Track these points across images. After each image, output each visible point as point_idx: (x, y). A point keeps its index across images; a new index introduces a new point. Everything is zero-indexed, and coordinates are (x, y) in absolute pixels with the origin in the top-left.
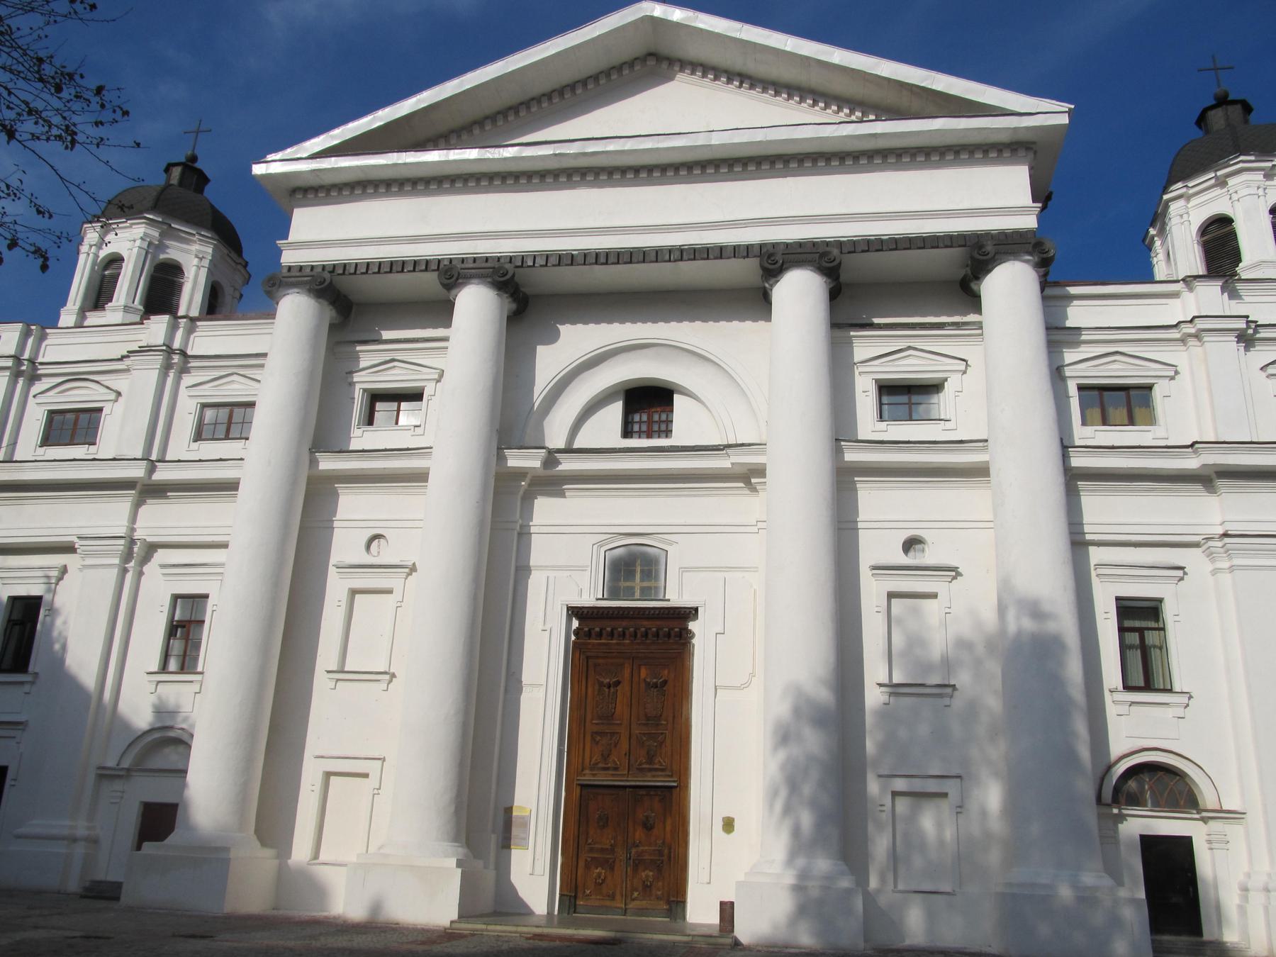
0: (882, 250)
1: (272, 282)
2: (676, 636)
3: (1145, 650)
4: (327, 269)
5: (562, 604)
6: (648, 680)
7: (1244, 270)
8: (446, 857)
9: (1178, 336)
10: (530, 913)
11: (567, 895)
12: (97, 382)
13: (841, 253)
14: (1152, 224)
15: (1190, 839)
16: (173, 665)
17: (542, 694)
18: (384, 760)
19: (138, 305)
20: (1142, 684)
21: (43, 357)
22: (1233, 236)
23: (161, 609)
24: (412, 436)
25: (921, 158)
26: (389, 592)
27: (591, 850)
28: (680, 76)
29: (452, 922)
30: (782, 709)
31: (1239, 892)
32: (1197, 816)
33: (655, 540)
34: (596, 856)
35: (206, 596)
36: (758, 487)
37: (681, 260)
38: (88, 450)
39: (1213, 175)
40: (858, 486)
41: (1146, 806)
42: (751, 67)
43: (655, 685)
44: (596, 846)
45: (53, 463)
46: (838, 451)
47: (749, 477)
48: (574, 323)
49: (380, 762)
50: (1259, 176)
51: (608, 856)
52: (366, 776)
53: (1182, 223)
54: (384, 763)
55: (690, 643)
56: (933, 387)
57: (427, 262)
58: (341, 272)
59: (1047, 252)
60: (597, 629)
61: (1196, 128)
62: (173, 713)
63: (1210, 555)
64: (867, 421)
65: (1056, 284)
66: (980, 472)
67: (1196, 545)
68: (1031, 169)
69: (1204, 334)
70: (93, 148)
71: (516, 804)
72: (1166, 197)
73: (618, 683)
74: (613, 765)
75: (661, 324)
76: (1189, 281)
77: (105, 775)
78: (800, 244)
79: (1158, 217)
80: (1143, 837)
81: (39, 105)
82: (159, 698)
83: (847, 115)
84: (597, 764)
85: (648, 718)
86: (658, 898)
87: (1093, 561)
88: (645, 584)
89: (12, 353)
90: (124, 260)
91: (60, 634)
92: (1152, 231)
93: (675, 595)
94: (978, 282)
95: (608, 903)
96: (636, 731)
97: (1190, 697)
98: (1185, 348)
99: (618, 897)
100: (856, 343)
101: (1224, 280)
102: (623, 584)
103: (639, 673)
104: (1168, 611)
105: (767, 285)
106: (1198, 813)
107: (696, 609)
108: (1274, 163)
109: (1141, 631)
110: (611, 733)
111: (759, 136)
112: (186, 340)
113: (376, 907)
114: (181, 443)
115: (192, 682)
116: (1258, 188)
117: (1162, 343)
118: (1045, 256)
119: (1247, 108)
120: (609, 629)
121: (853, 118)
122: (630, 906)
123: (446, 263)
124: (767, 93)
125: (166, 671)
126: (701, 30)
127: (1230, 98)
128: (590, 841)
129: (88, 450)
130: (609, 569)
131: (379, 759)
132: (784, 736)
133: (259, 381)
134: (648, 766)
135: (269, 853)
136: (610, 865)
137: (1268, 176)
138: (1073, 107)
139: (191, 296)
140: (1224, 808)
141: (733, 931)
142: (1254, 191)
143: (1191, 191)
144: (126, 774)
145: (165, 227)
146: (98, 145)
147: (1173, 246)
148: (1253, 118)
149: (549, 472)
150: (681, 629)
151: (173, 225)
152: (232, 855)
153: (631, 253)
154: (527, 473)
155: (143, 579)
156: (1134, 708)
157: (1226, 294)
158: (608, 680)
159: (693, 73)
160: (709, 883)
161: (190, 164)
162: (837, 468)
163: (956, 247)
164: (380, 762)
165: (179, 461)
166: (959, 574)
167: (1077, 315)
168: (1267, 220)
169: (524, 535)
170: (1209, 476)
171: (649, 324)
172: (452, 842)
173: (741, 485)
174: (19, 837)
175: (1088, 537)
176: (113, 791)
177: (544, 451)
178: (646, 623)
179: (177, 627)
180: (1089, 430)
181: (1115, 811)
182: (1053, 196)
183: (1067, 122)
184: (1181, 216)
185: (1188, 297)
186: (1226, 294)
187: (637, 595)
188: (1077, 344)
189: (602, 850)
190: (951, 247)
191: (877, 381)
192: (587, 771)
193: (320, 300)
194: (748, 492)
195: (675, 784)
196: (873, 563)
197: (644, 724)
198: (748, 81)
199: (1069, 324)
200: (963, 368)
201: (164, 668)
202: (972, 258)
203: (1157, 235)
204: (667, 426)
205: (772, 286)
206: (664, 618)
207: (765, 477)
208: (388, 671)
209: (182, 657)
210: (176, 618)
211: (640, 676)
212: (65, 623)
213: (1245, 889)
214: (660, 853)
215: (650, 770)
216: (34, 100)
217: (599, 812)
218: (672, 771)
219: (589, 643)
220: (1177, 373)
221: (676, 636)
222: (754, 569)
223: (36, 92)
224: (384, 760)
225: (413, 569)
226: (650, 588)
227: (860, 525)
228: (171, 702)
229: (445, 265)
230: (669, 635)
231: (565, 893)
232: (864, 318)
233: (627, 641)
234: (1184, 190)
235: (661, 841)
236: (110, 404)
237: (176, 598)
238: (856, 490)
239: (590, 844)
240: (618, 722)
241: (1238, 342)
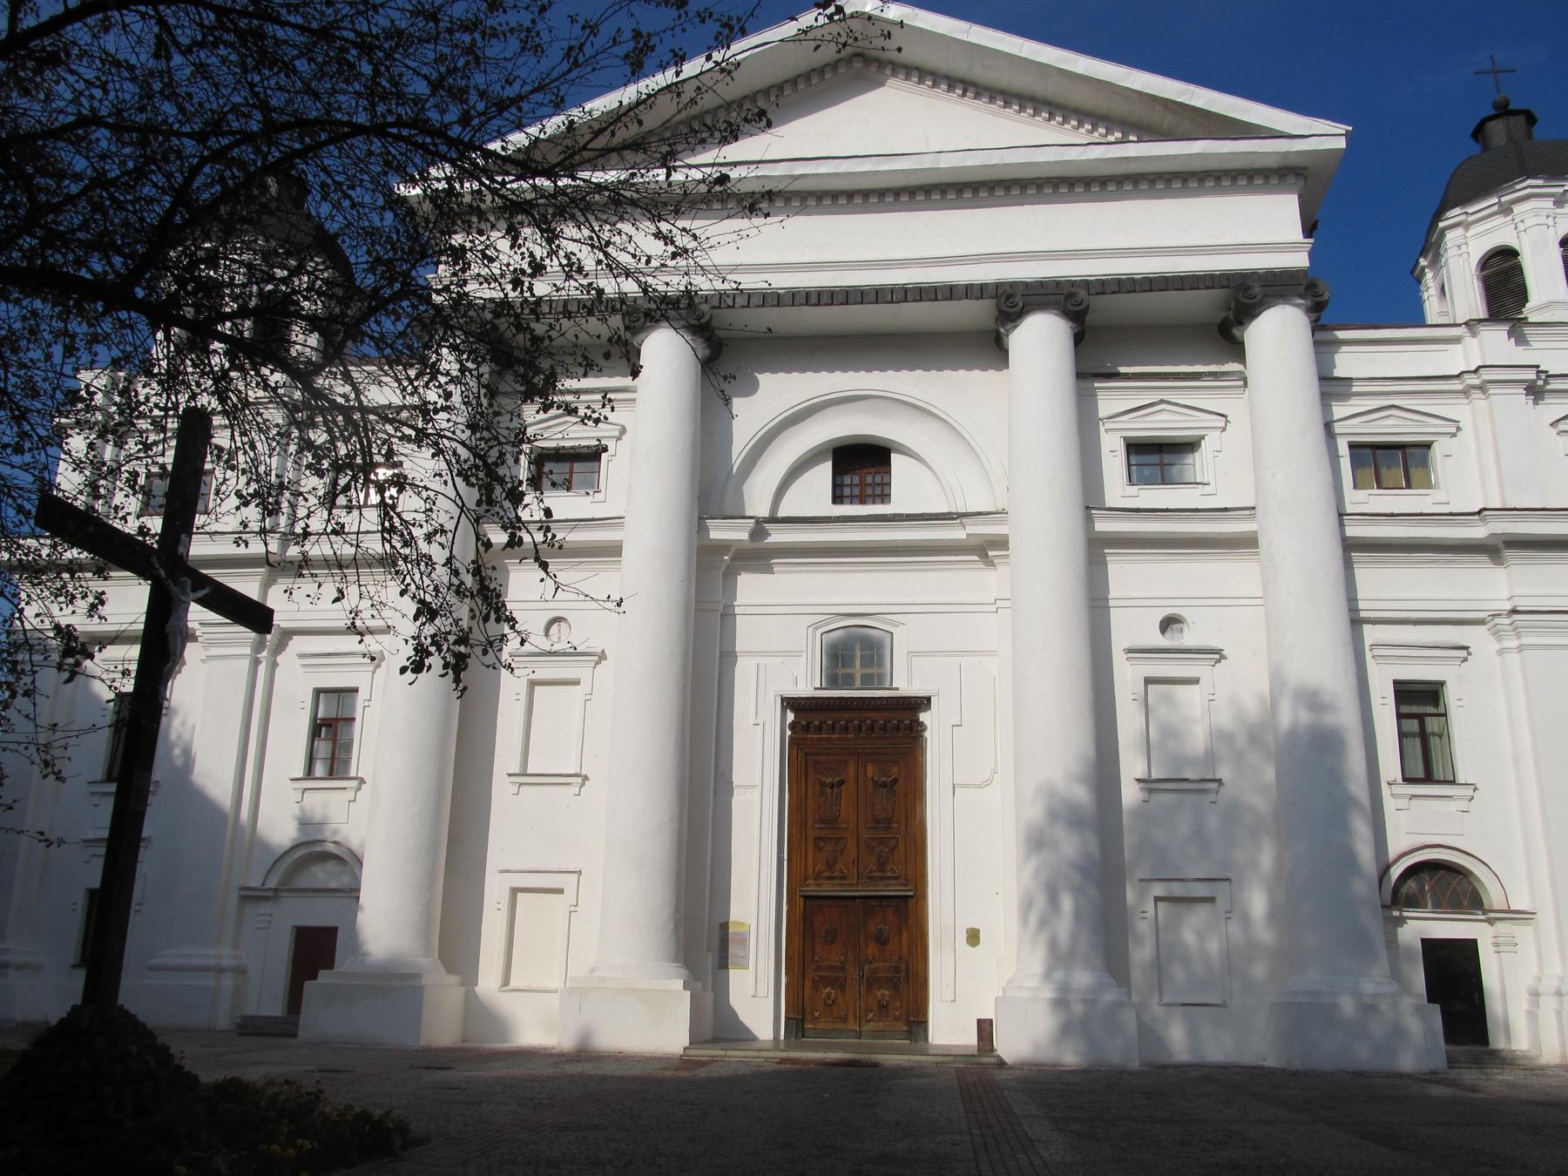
0: (1135, 291)
2: (906, 729)
3: (1424, 736)
5: (775, 695)
7: (1532, 313)
8: (669, 978)
9: (1460, 387)
10: (754, 1038)
13: (1089, 294)
14: (1423, 253)
15: (1474, 942)
16: (320, 769)
17: (757, 797)
18: (580, 873)
20: (1421, 775)
22: (1518, 270)
23: (303, 705)
25: (1177, 185)
26: (576, 682)
27: (819, 968)
28: (891, 82)
29: (685, 1049)
30: (1035, 812)
31: (1528, 997)
32: (1483, 917)
34: (824, 974)
35: (356, 690)
36: (995, 561)
37: (906, 301)
39: (1496, 200)
40: (1108, 558)
41: (1426, 907)
42: (978, 73)
43: (884, 785)
44: (824, 963)
46: (1089, 520)
47: (986, 550)
48: (774, 371)
49: (576, 875)
50: (1548, 203)
51: (837, 975)
52: (560, 891)
53: (1460, 255)
55: (922, 736)
56: (1188, 446)
60: (817, 723)
61: (1471, 141)
62: (321, 825)
63: (1497, 633)
64: (1117, 487)
65: (1324, 328)
66: (1246, 543)
67: (1481, 622)
69: (1489, 386)
71: (732, 919)
72: (1441, 225)
73: (842, 783)
75: (876, 373)
76: (1472, 325)
77: (249, 897)
78: (1042, 284)
79: (1430, 245)
80: (1425, 942)
82: (302, 809)
83: (1088, 131)
85: (878, 822)
86: (896, 1019)
87: (1368, 642)
91: (179, 736)
92: (1423, 262)
93: (904, 683)
95: (840, 1026)
96: (865, 836)
97: (1475, 789)
98: (1466, 401)
99: (851, 1018)
100: (1101, 395)
101: (1511, 324)
102: (840, 671)
103: (866, 771)
104: (1451, 696)
105: (1002, 330)
106: (1483, 914)
107: (929, 699)
108: (1566, 188)
109: (1420, 717)
111: (995, 159)
113: (586, 1037)
115: (345, 789)
116: (1548, 217)
117: (1447, 396)
118: (1318, 299)
119: (1531, 119)
120: (830, 722)
121: (1111, 138)
124: (995, 103)
127: (1512, 107)
128: (817, 958)
130: (827, 654)
131: (574, 872)
132: (1036, 842)
134: (879, 874)
135: (453, 979)
136: (839, 983)
137: (1559, 202)
138: (1350, 128)
140: (1512, 908)
142: (1543, 220)
143: (1471, 218)
144: (275, 895)
148: (1536, 129)
149: (756, 545)
150: (912, 721)
152: (424, 982)
153: (847, 292)
155: (278, 670)
156: (1414, 802)
157: (1513, 339)
158: (830, 780)
159: (921, 82)
160: (954, 1001)
166: (1223, 657)
167: (1347, 363)
168: (1556, 253)
169: (728, 616)
170: (1496, 546)
171: (851, 373)
173: (976, 558)
174: (152, 969)
175: (1363, 614)
176: (259, 915)
177: (753, 521)
178: (871, 714)
179: (321, 726)
180: (1362, 494)
181: (1396, 913)
182: (1319, 226)
183: (1344, 146)
184: (1459, 247)
185: (1471, 343)
186: (1513, 339)
187: (858, 683)
188: (1346, 396)
189: (831, 968)
190: (1213, 288)
191: (1125, 438)
192: (810, 882)
194: (983, 566)
195: (911, 894)
196: (1126, 646)
197: (874, 828)
198: (974, 90)
199: (1337, 373)
201: (309, 773)
203: (1429, 266)
206: (893, 709)
207: (1008, 550)
210: (319, 716)
211: (866, 775)
212: (184, 724)
213: (1535, 994)
214: (897, 970)
215: (882, 878)
219: (808, 739)
220: (1459, 429)
221: (906, 729)
222: (993, 653)
224: (580, 873)
225: (602, 656)
226: (872, 675)
227: (1111, 603)
228: (318, 815)
230: (846, 729)
231: (791, 1016)
232: (1108, 367)
234: (1463, 217)
237: (318, 692)
238: (1105, 563)
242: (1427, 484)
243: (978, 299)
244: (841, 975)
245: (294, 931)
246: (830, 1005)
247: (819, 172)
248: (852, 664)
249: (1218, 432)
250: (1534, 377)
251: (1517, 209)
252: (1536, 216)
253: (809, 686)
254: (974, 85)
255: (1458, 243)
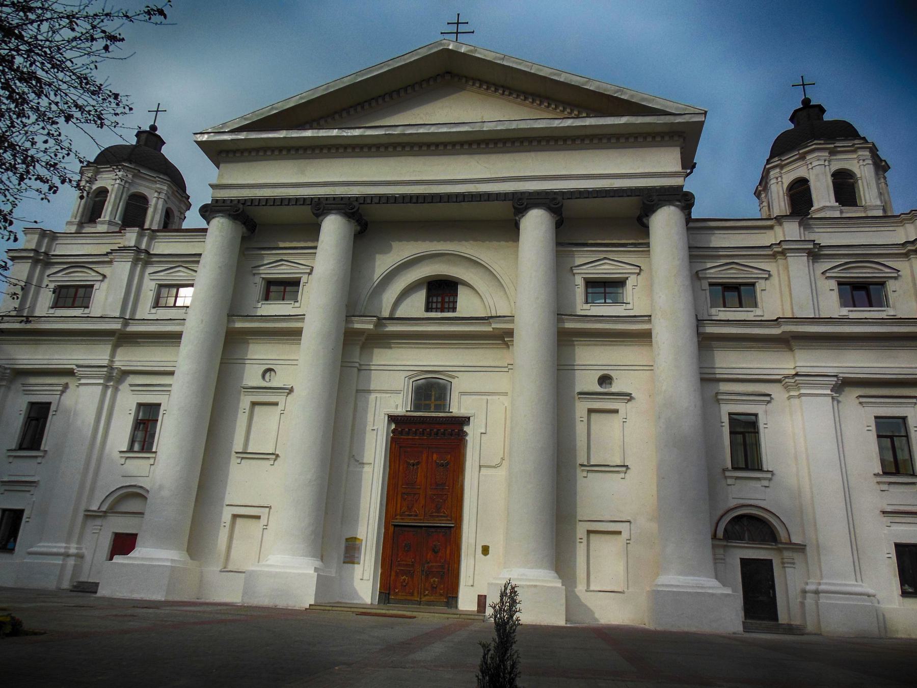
1: (205, 209)
4: (241, 202)
6: (438, 461)
9: (771, 253)
11: (383, 593)
12: (91, 269)
17: (371, 470)
19: (118, 220)
21: (153, 250)
22: (808, 190)
24: (293, 307)
33: (444, 375)
35: (159, 405)
36: (509, 343)
37: (464, 201)
38: (84, 311)
39: (797, 153)
44: (403, 563)
45: (73, 318)
54: (271, 510)
57: (304, 199)
58: (250, 204)
59: (689, 200)
67: (778, 381)
68: (682, 148)
70: (112, 128)
73: (418, 463)
74: (415, 514)
76: (779, 219)
77: (90, 516)
81: (80, 102)
84: (404, 512)
86: (441, 595)
88: (438, 402)
89: (33, 247)
90: (108, 191)
93: (457, 407)
94: (647, 218)
95: (409, 598)
97: (773, 475)
99: (416, 594)
105: (517, 218)
107: (469, 418)
110: (414, 494)
112: (149, 244)
114: (145, 310)
116: (825, 161)
117: (747, 257)
118: (688, 202)
120: (414, 430)
121: (573, 115)
122: (423, 600)
123: (317, 200)
125: (132, 450)
126: (479, 58)
129: (84, 311)
130: (415, 392)
133: (196, 271)
139: (153, 218)
141: (485, 613)
145: (136, 171)
146: (115, 127)
147: (772, 197)
151: (141, 171)
153: (432, 196)
154: (364, 332)
156: (738, 481)
161: (152, 132)
162: (558, 332)
163: (625, 197)
164: (268, 509)
165: (144, 320)
172: (312, 557)
174: (30, 553)
176: (95, 526)
177: (375, 318)
184: (777, 178)
185: (778, 229)
190: (631, 196)
191: (584, 278)
192: (398, 517)
193: (236, 221)
200: (638, 271)
201: (131, 449)
202: (644, 203)
204: (454, 305)
205: (520, 218)
208: (274, 452)
209: (142, 443)
211: (433, 459)
215: (438, 516)
216: (78, 99)
217: (405, 542)
218: (451, 517)
223: (79, 95)
229: (315, 201)
230: (423, 434)
233: (425, 437)
234: (779, 162)
235: (443, 560)
236: (99, 283)
237: (140, 405)
239: (399, 561)
240: (419, 487)
241: (808, 256)
242: (755, 305)
243: (503, 201)
244: (412, 569)
245: (113, 536)
246: (405, 586)
247: (418, 132)
248: (430, 399)
249: (635, 276)
250: (812, 247)
251: (808, 157)
252: (818, 160)
253: (404, 410)
254: (509, 88)
255: (777, 176)
